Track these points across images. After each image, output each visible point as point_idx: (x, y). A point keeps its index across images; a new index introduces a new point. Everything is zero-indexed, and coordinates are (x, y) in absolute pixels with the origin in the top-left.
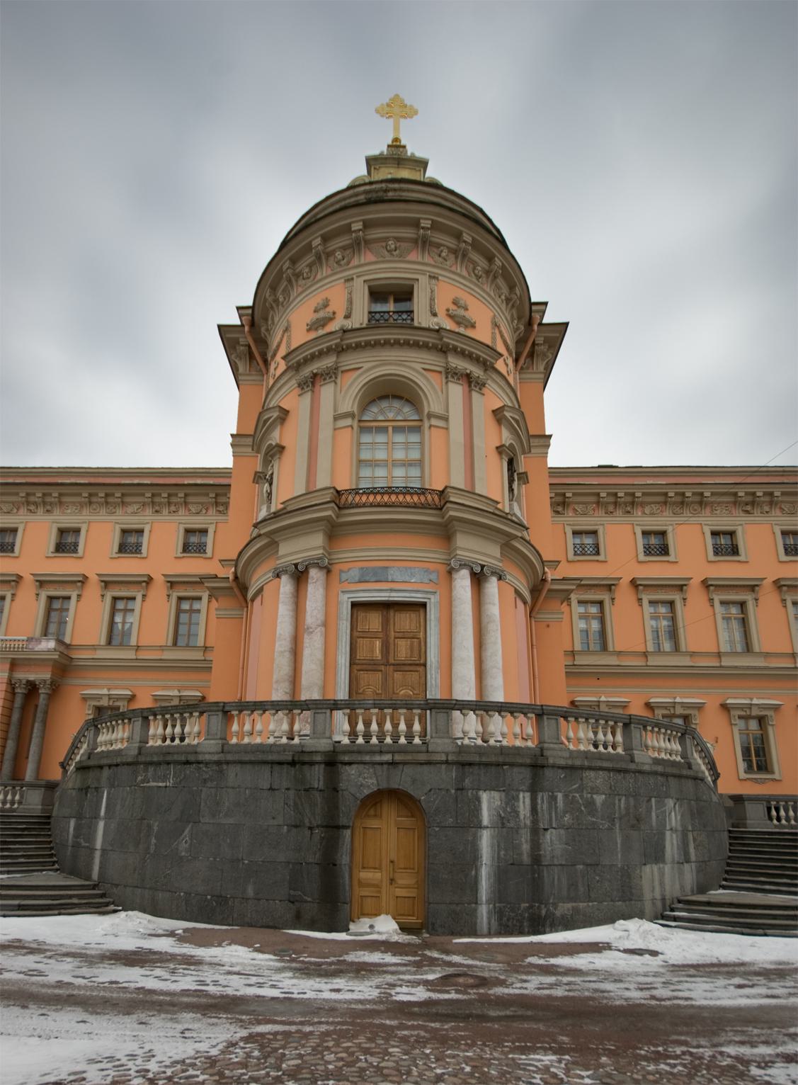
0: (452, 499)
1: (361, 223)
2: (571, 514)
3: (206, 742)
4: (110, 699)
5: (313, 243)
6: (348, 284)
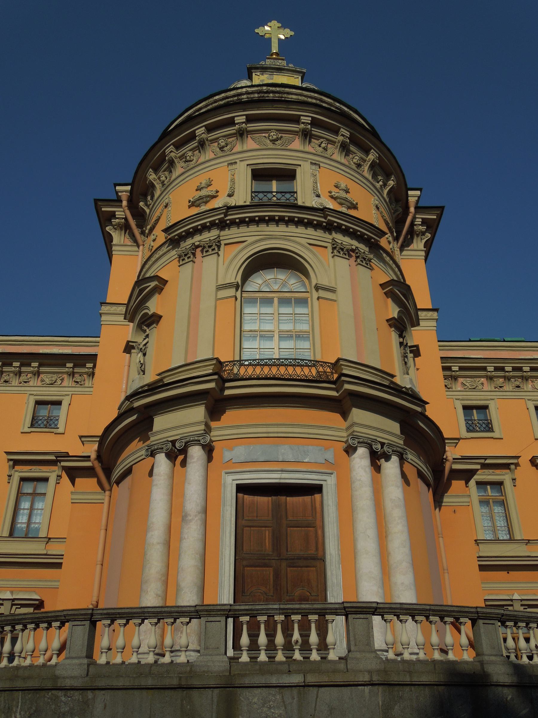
0: (345, 372)
1: (245, 117)
2: (459, 389)
3: (68, 661)
4: (13, 605)
5: (197, 132)
6: (230, 167)
